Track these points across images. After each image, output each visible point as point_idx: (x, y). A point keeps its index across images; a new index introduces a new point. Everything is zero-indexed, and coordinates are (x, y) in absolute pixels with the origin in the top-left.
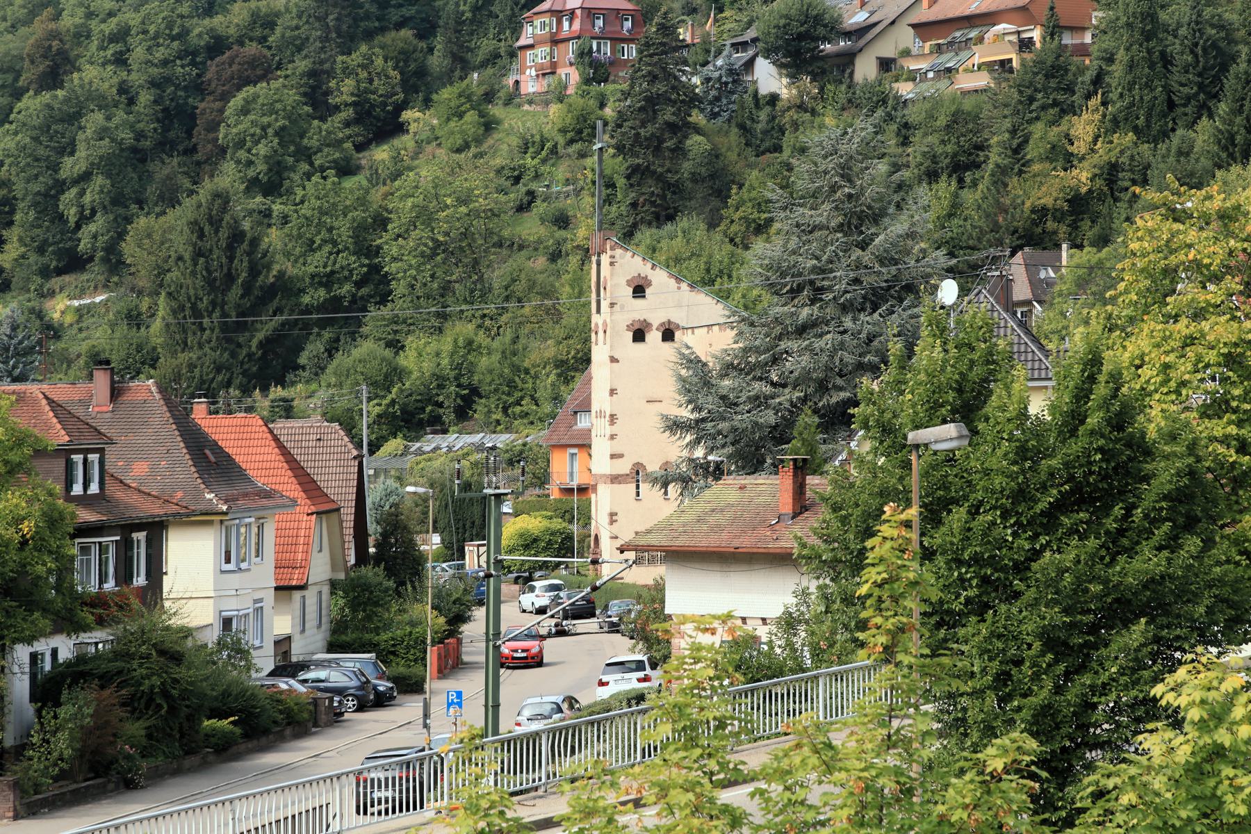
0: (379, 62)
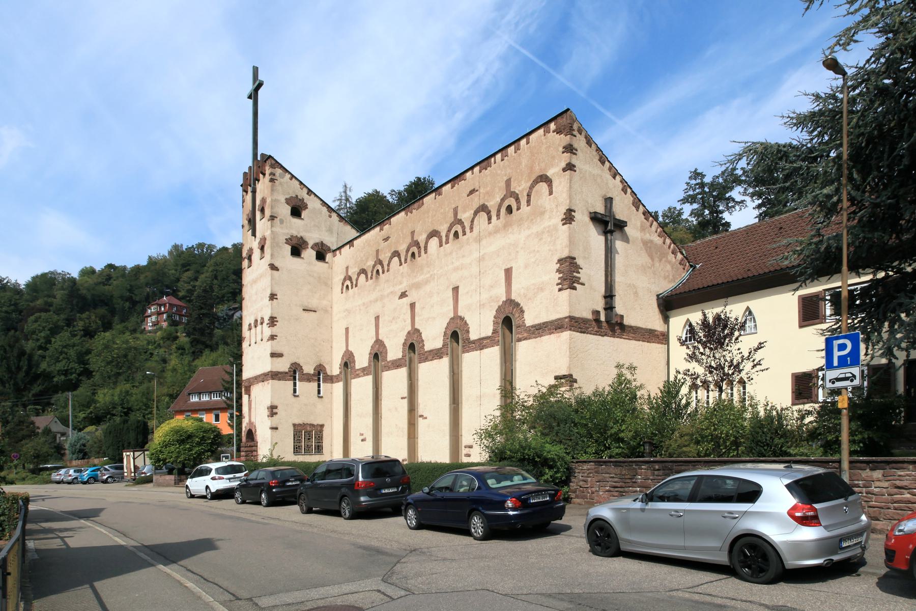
0: (93, 317)
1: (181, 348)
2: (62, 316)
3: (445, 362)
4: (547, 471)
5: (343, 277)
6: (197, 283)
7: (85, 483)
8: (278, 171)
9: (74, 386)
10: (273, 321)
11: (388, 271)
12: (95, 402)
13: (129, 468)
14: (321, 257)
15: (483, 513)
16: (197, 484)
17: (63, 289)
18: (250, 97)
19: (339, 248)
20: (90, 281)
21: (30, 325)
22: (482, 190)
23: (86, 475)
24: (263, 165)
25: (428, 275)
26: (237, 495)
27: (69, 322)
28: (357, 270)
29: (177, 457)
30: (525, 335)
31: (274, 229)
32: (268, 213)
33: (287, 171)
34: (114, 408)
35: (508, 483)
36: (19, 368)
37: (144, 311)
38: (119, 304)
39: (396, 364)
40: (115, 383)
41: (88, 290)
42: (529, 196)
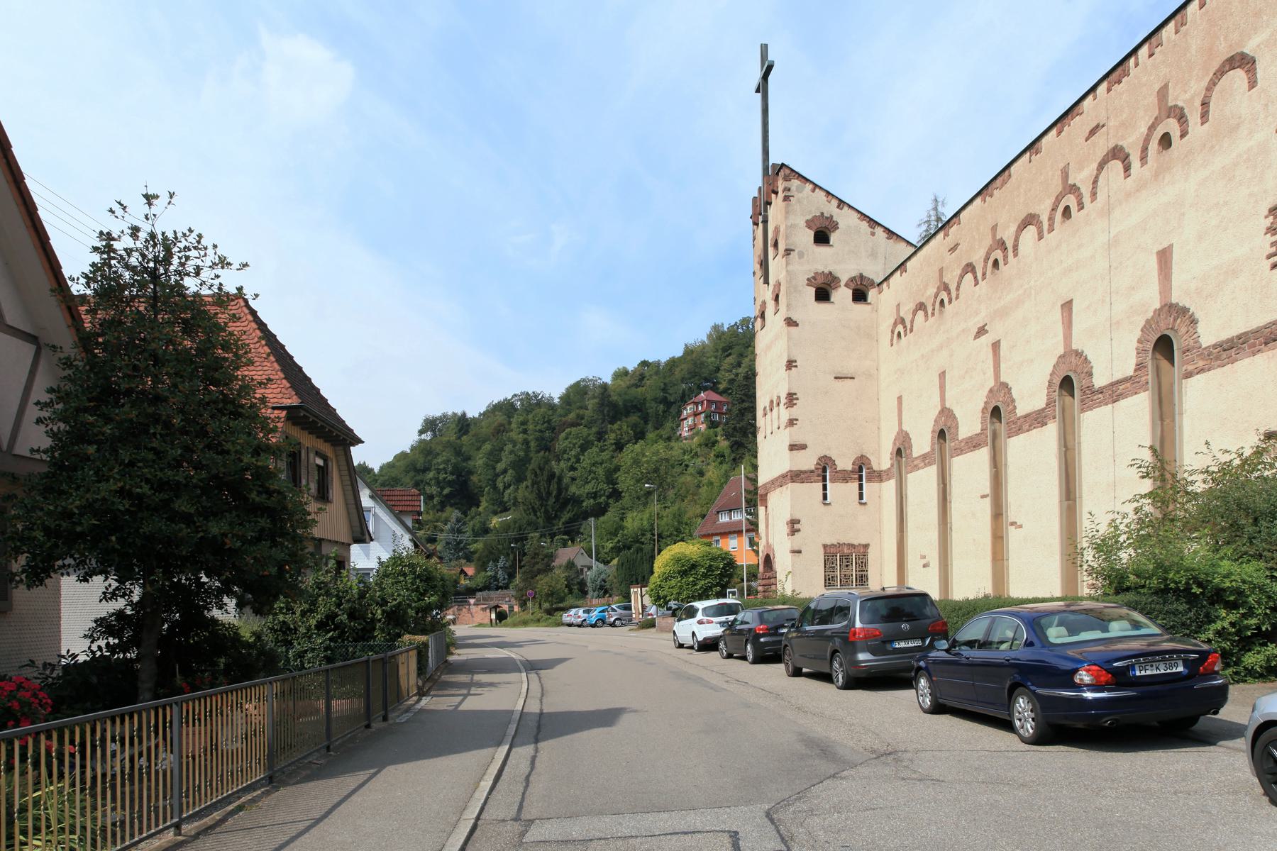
1: (720, 456)
2: (594, 430)
3: (1051, 432)
4: (1223, 613)
5: (892, 321)
6: (740, 370)
7: (593, 626)
8: (795, 183)
9: (600, 511)
10: (791, 399)
11: (957, 298)
12: (622, 528)
13: (637, 609)
14: (860, 296)
15: (1034, 692)
16: (687, 629)
17: (594, 397)
18: (758, 91)
19: (886, 279)
20: (623, 384)
21: (561, 444)
22: (1112, 123)
23: (595, 615)
24: (777, 176)
25: (1021, 292)
26: (722, 645)
27: (601, 436)
28: (912, 306)
29: (679, 593)
30: (1201, 363)
31: (790, 268)
32: (782, 247)
33: (807, 180)
34: (643, 535)
35: (1097, 635)
36: (549, 494)
37: (680, 413)
38: (652, 408)
39: (973, 444)
40: (645, 505)
41: (620, 395)
42: (1205, 104)
